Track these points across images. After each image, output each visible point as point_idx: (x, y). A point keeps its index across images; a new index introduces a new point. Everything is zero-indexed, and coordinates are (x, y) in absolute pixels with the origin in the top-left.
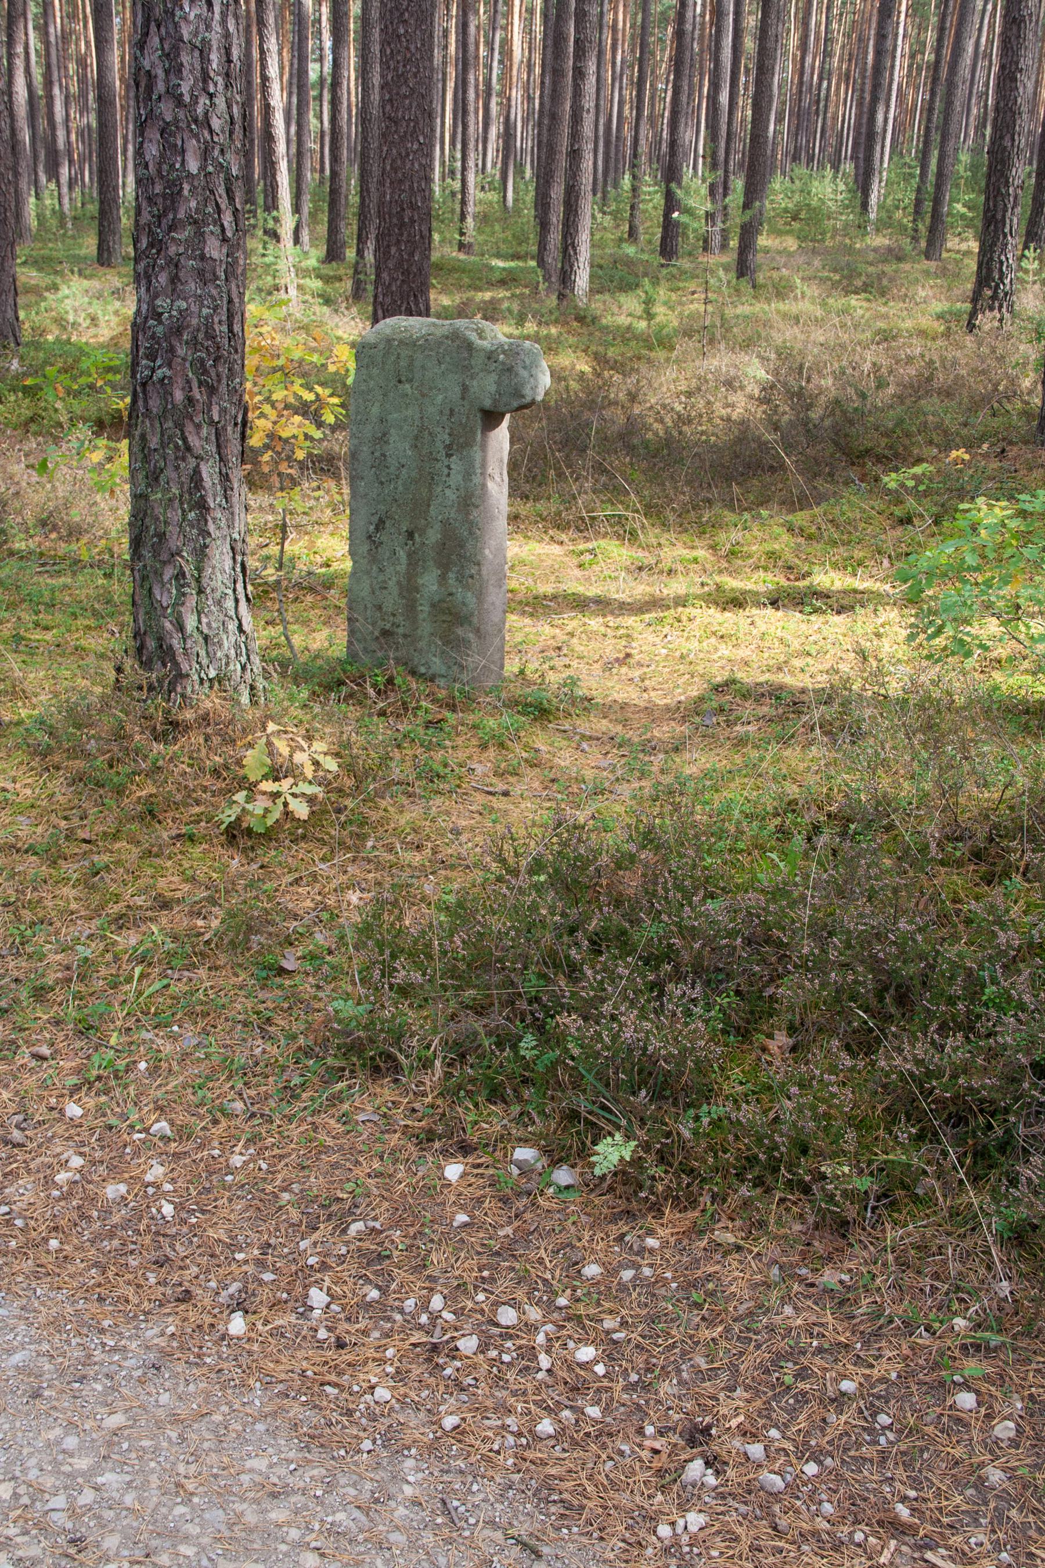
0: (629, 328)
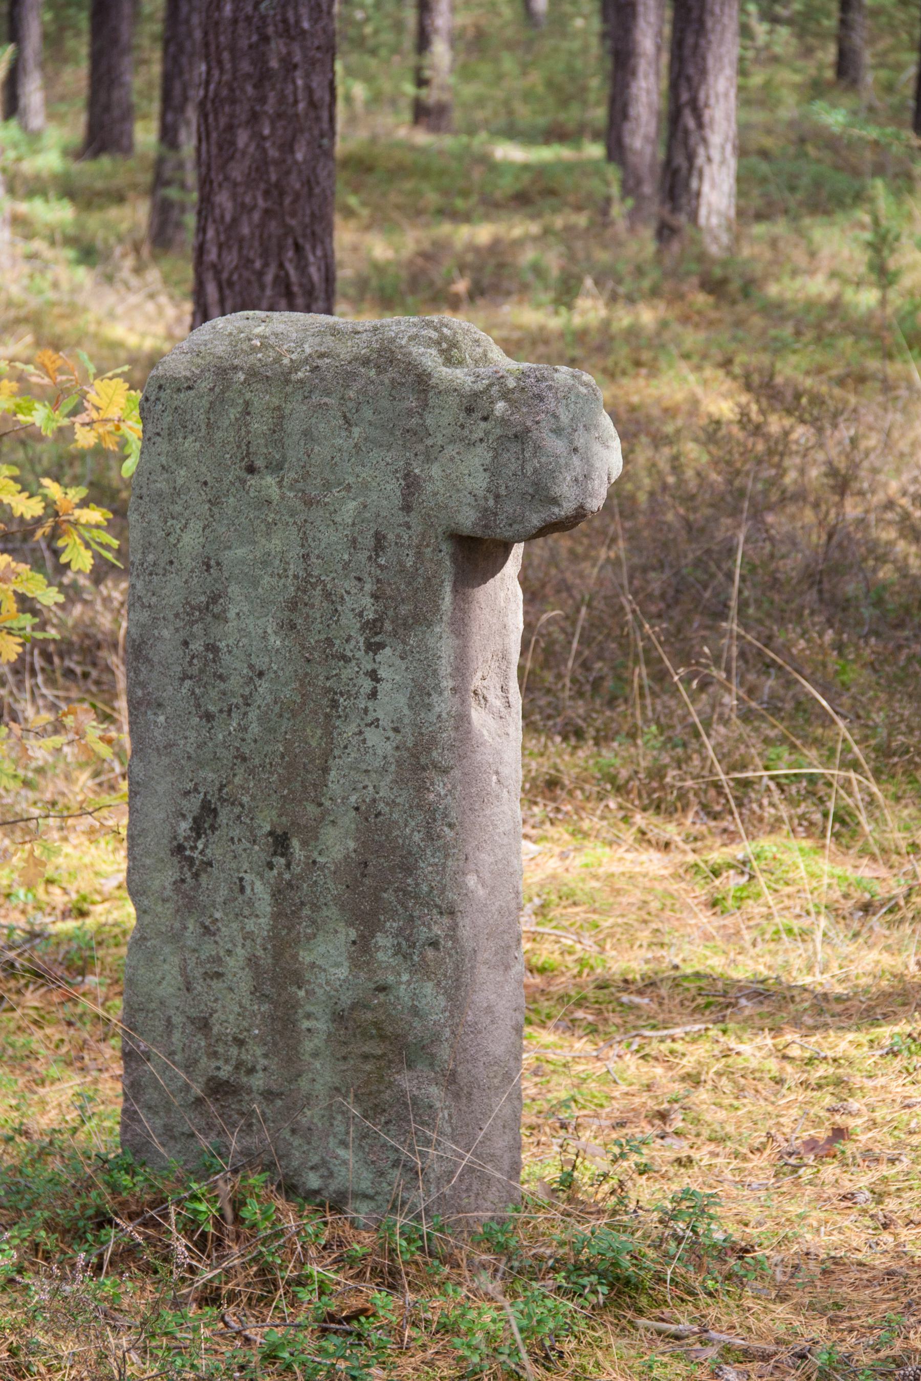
0: (835, 306)
